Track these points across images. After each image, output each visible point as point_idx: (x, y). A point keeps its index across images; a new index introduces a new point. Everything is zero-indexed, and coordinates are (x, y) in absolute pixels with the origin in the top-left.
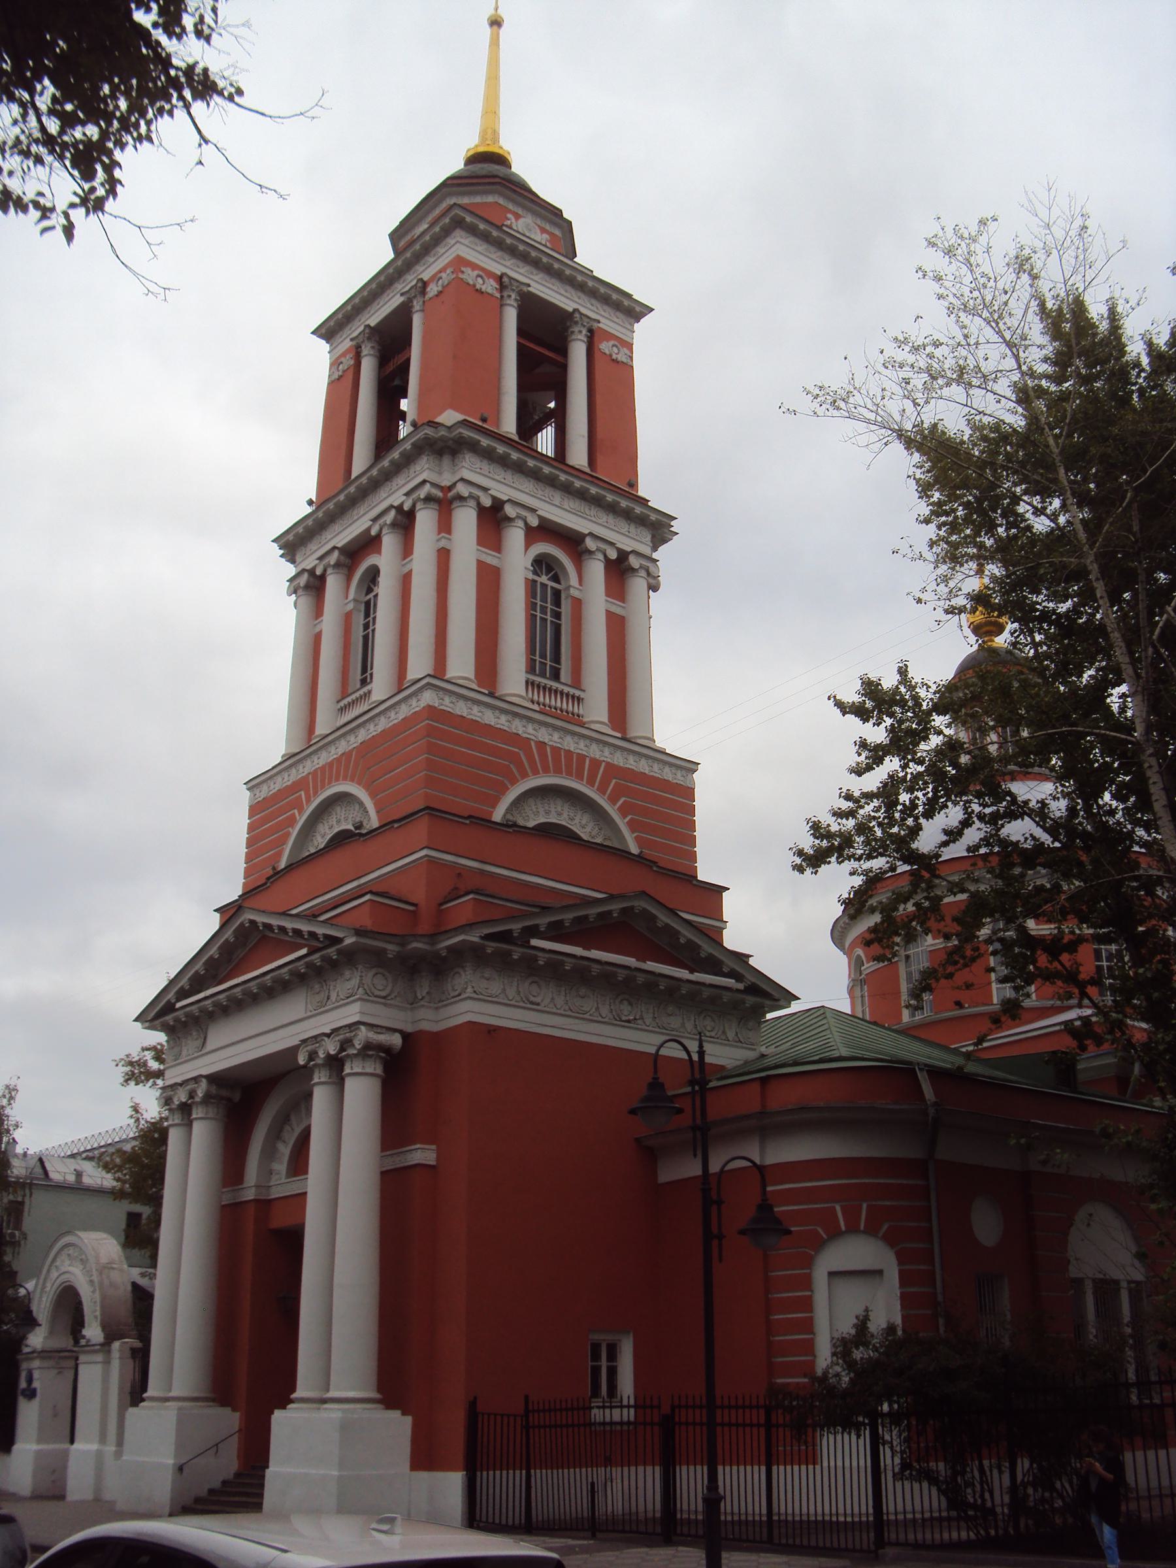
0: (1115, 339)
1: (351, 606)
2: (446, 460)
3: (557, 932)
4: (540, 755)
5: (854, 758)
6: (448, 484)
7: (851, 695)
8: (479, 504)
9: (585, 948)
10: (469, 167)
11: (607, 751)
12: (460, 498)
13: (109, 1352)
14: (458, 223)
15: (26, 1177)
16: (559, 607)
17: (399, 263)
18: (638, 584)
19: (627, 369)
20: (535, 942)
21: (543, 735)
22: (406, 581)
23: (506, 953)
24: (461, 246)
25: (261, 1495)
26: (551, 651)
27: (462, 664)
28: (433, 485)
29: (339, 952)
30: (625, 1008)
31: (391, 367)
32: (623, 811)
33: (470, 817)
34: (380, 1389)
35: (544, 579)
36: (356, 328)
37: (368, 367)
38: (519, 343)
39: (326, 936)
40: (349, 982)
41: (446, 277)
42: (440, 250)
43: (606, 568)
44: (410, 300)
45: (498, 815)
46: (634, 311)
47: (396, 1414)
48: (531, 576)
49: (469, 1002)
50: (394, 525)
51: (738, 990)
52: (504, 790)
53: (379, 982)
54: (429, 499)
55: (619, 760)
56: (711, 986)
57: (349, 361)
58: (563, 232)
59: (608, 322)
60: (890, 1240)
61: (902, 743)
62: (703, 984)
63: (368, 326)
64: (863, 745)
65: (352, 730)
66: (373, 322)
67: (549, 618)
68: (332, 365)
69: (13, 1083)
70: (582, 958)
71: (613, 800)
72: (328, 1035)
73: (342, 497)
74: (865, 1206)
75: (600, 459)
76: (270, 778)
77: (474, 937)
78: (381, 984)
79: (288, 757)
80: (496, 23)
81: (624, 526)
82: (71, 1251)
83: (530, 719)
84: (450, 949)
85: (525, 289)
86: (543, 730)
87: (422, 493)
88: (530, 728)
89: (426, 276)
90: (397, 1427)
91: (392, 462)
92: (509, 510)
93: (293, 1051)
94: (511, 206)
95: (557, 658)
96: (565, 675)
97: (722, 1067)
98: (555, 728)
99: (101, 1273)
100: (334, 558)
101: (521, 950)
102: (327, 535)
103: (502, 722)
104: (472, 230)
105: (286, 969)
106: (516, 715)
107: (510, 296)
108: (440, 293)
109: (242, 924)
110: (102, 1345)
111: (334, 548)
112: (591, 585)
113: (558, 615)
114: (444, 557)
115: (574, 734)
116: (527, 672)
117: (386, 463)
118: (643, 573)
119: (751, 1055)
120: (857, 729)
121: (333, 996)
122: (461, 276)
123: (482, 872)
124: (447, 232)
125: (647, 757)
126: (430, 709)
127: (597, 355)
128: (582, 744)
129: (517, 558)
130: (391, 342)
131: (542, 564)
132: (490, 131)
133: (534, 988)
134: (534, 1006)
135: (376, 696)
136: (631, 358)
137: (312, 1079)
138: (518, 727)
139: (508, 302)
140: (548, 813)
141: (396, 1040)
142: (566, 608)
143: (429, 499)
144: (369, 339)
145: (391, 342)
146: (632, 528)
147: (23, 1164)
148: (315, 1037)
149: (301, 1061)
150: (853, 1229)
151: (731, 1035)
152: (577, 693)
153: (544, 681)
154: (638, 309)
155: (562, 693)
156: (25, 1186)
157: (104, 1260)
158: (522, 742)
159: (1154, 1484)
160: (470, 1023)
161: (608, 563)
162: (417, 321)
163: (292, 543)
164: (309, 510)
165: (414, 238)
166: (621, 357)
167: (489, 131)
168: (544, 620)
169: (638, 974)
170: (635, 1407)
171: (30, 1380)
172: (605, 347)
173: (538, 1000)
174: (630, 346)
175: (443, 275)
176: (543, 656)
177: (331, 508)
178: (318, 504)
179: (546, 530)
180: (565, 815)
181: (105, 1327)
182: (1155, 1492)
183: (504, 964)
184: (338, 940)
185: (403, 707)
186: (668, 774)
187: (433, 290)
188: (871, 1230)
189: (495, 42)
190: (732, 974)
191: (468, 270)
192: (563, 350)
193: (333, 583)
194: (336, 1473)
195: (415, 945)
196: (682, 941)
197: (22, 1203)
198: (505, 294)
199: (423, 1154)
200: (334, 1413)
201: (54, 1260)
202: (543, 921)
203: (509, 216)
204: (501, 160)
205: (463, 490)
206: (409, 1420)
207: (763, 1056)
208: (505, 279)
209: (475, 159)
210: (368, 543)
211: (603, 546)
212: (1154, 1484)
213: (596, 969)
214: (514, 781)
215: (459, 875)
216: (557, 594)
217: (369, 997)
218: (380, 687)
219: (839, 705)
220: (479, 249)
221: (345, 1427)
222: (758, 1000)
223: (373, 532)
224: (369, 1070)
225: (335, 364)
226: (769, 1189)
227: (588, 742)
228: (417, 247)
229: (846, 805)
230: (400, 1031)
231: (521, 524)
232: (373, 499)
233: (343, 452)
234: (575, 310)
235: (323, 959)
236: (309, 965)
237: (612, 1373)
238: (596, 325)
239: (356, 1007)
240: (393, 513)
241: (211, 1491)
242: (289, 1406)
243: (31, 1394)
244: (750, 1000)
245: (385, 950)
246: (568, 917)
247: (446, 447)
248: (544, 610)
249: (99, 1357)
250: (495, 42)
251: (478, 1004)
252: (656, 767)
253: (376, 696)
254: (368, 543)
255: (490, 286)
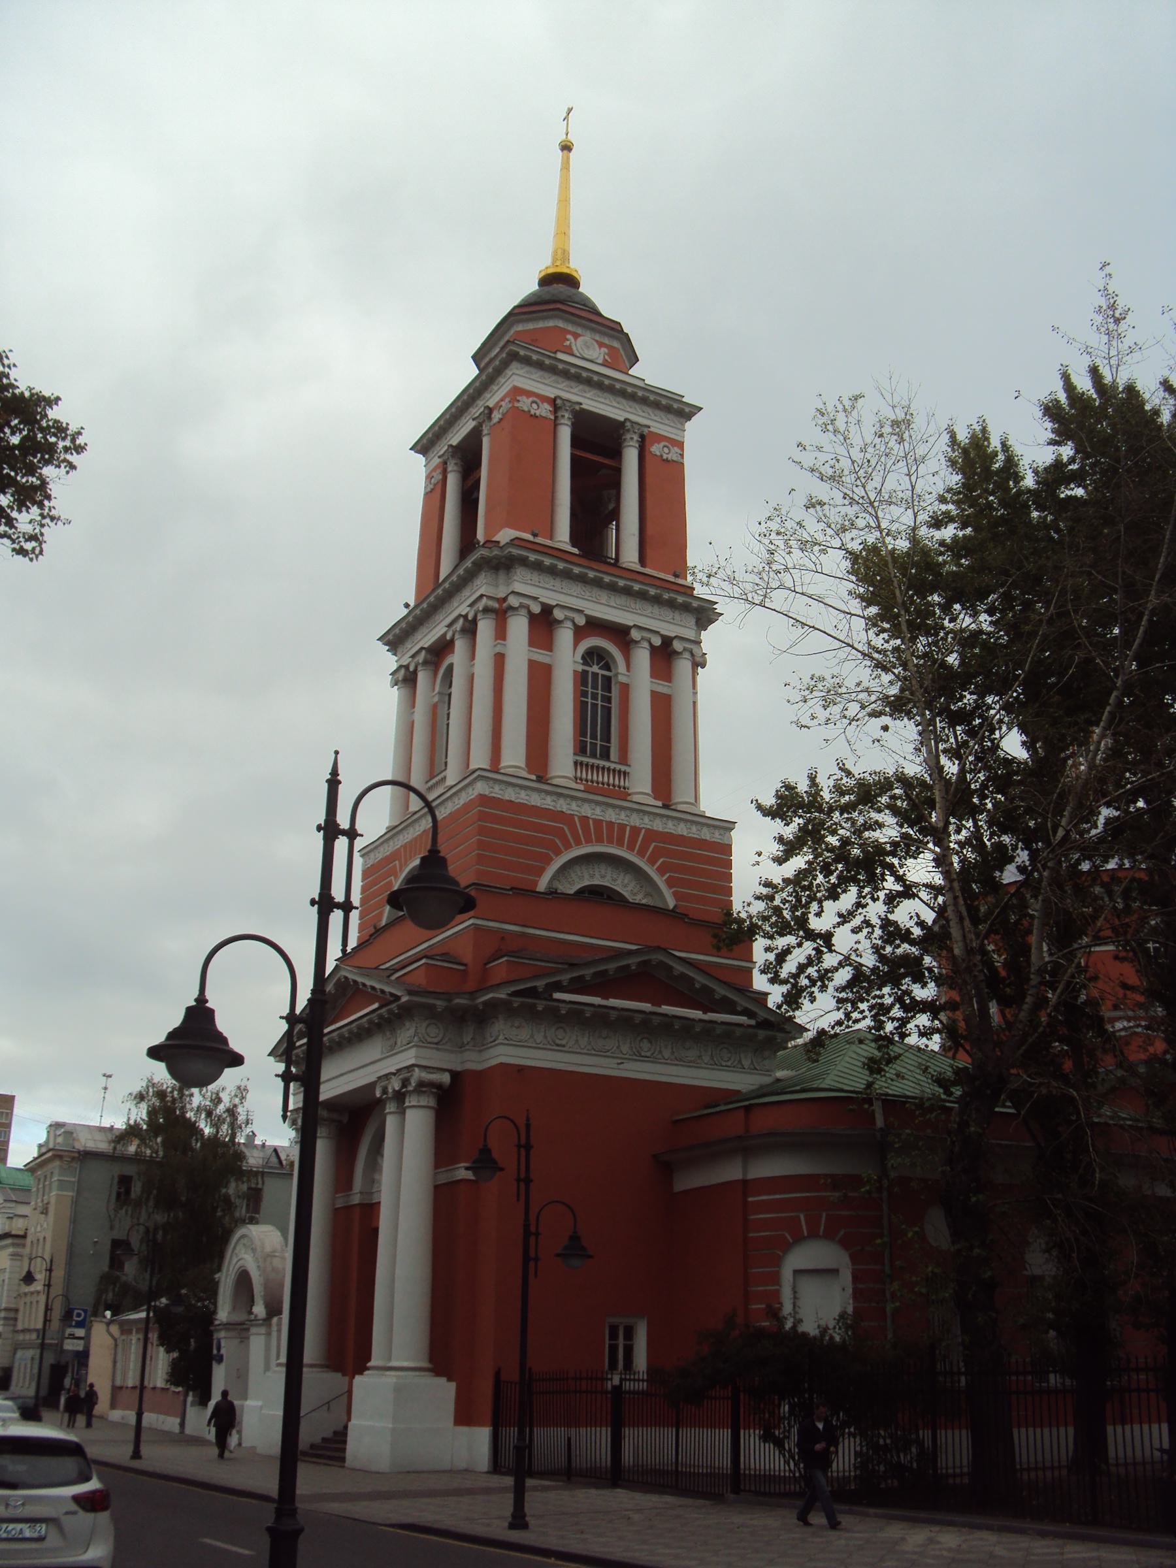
0: (1011, 467)
1: (436, 699)
2: (502, 576)
3: (579, 986)
4: (572, 835)
5: (776, 849)
6: (503, 595)
7: (769, 801)
8: (529, 612)
9: (603, 998)
10: (546, 288)
11: (646, 819)
12: (511, 608)
13: (270, 1325)
14: (514, 357)
15: (263, 1167)
16: (610, 692)
17: (484, 377)
18: (683, 666)
19: (675, 472)
20: (557, 995)
21: (587, 810)
22: (471, 678)
23: (532, 1007)
24: (518, 377)
25: (345, 1442)
26: (599, 730)
27: (514, 755)
28: (489, 597)
29: (399, 1007)
30: (645, 1045)
31: (470, 483)
32: (661, 871)
33: (512, 889)
34: (431, 1360)
35: (595, 669)
36: (442, 448)
37: (453, 481)
38: (572, 455)
39: (392, 994)
40: (407, 1032)
41: (505, 405)
42: (502, 380)
43: (651, 654)
44: (480, 425)
45: (542, 885)
46: (682, 411)
47: (442, 1380)
48: (580, 668)
49: (501, 1047)
50: (464, 631)
51: (750, 1026)
52: (549, 861)
53: (433, 1031)
54: (487, 610)
55: (658, 825)
56: (723, 1023)
57: (438, 476)
58: (622, 345)
59: (658, 424)
60: (845, 1244)
61: (810, 836)
62: (715, 1022)
63: (451, 446)
64: (781, 840)
65: (455, 794)
66: (455, 441)
67: (600, 703)
68: (427, 477)
69: (243, 1084)
70: (600, 1006)
71: (652, 861)
72: (394, 1074)
73: (432, 599)
74: (824, 1215)
75: (649, 553)
76: (376, 848)
77: (502, 995)
78: (434, 1032)
79: (390, 829)
80: (566, 147)
81: (668, 614)
82: (245, 1241)
83: (573, 798)
84: (485, 1003)
85: (577, 408)
86: (586, 806)
87: (480, 606)
88: (574, 806)
89: (491, 404)
90: (445, 1391)
91: (466, 570)
92: (558, 614)
93: (371, 1086)
94: (570, 328)
95: (607, 737)
96: (614, 755)
97: (739, 1091)
98: (598, 803)
99: (265, 1260)
100: (421, 658)
101: (544, 1002)
102: (418, 635)
103: (548, 802)
104: (527, 361)
105: (365, 1020)
106: (560, 795)
107: (563, 416)
108: (501, 420)
109: (339, 979)
110: (264, 1320)
111: (422, 648)
112: (638, 674)
113: (609, 700)
114: (500, 660)
115: (614, 806)
116: (575, 754)
117: (468, 563)
118: (687, 655)
119: (767, 1080)
120: (776, 827)
121: (399, 1043)
122: (517, 404)
123: (524, 934)
124: (505, 365)
125: (686, 821)
126: (483, 799)
127: (648, 458)
128: (623, 815)
129: (566, 656)
130: (468, 457)
131: (593, 655)
132: (562, 253)
133: (560, 1033)
134: (560, 1047)
135: (450, 782)
136: (682, 456)
137: (384, 1109)
138: (562, 805)
139: (562, 421)
140: (592, 876)
141: (446, 1078)
142: (615, 693)
143: (487, 610)
144: (453, 456)
145: (468, 457)
146: (677, 615)
147: (261, 1155)
148: (386, 1075)
149: (378, 1095)
150: (813, 1235)
151: (746, 1063)
152: (623, 768)
153: (591, 761)
154: (687, 410)
155: (609, 769)
156: (260, 1174)
157: (268, 1249)
158: (567, 818)
159: (1121, 1454)
160: (502, 1065)
161: (654, 650)
162: (486, 441)
163: (395, 639)
164: (406, 611)
165: (498, 353)
166: (672, 456)
167: (559, 252)
168: (595, 706)
169: (653, 1017)
170: (647, 1381)
171: (219, 1349)
172: (656, 449)
173: (564, 1042)
174: (681, 445)
175: (503, 403)
176: (594, 736)
177: (433, 597)
178: (421, 597)
179: (595, 626)
180: (608, 877)
181: (267, 1306)
182: (1121, 1461)
183: (531, 1015)
184: (398, 998)
185: (463, 794)
186: (706, 834)
187: (496, 416)
188: (829, 1235)
189: (566, 166)
190: (750, 1014)
191: (523, 399)
192: (616, 454)
193: (422, 677)
194: (390, 1426)
195: (457, 1001)
196: (697, 986)
197: (260, 1190)
198: (560, 414)
199: (462, 1173)
200: (391, 1378)
201: (235, 1248)
202: (565, 978)
203: (569, 337)
204: (570, 281)
205: (514, 601)
206: (453, 1385)
207: (778, 1080)
208: (559, 402)
209: (547, 280)
210: (441, 649)
211: (647, 635)
212: (1121, 1454)
213: (613, 1015)
214: (558, 852)
215: (503, 938)
216: (608, 682)
217: (423, 1043)
218: (452, 775)
219: (759, 807)
220: (533, 377)
221: (398, 1389)
222: (770, 1033)
223: (448, 637)
224: (422, 1104)
225: (429, 477)
226: (750, 1199)
227: (628, 812)
228: (497, 362)
229: (765, 891)
230: (450, 1071)
231: (569, 624)
232: (448, 608)
233: (434, 558)
234: (626, 420)
235: (389, 1011)
236: (381, 1017)
237: (629, 1351)
238: (646, 431)
239: (412, 1052)
240: (461, 621)
241: (324, 1440)
242: (367, 1372)
243: (220, 1359)
244: (762, 1034)
245: (435, 1005)
246: (588, 972)
247: (503, 564)
248: (595, 696)
249: (263, 1330)
250: (566, 166)
251: (513, 1048)
252: (694, 828)
253: (450, 782)
254: (441, 649)
255: (545, 410)
